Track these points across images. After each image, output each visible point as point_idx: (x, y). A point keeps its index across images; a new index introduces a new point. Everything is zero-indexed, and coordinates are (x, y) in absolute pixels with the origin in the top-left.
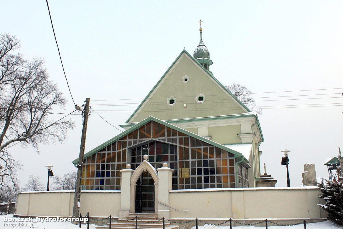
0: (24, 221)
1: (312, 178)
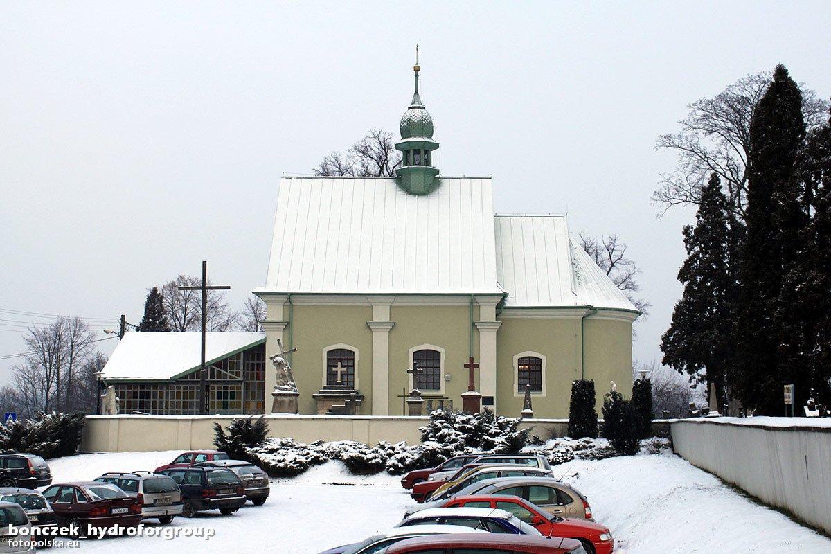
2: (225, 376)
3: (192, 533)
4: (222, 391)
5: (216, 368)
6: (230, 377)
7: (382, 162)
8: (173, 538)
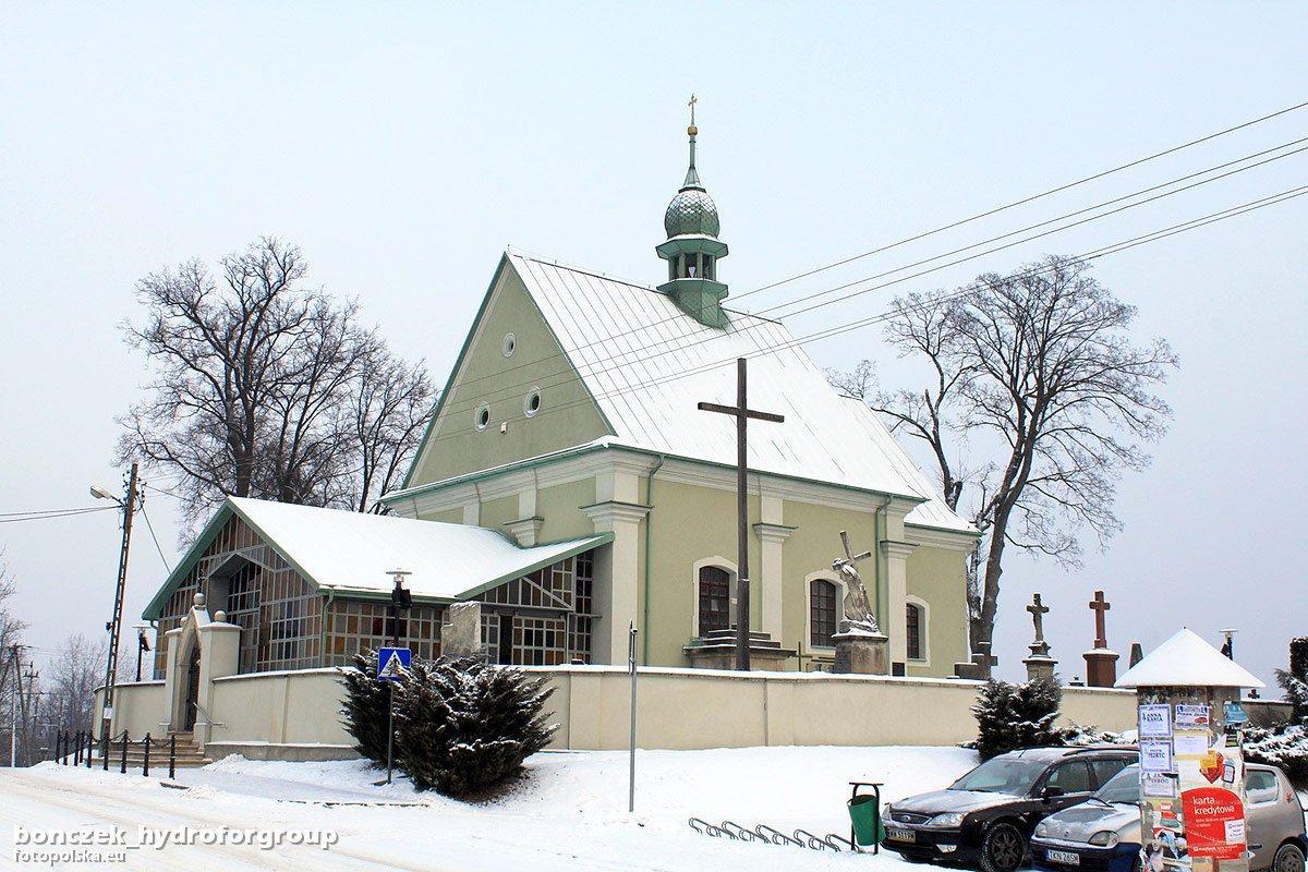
0: (91, 843)
1: (461, 643)
2: (547, 598)
3: (215, 840)
4: (534, 629)
5: (533, 584)
6: (556, 604)
7: (1008, 284)
8: (272, 847)
